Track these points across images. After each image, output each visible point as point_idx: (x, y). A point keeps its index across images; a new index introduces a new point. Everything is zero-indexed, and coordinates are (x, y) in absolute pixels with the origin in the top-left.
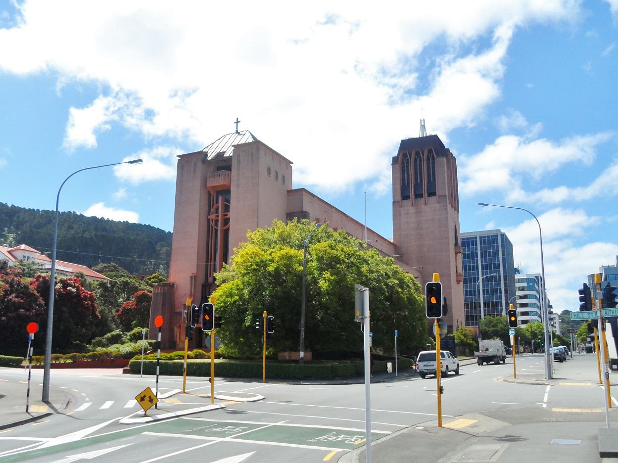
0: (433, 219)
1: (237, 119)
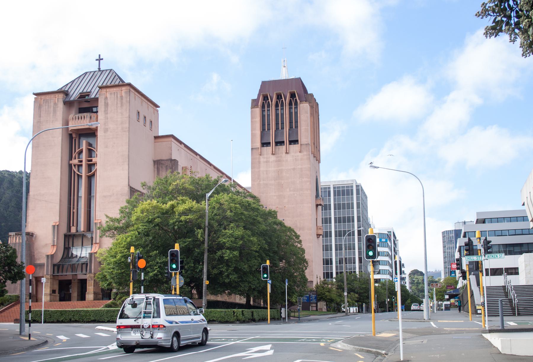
0: (294, 169)
1: (100, 55)
